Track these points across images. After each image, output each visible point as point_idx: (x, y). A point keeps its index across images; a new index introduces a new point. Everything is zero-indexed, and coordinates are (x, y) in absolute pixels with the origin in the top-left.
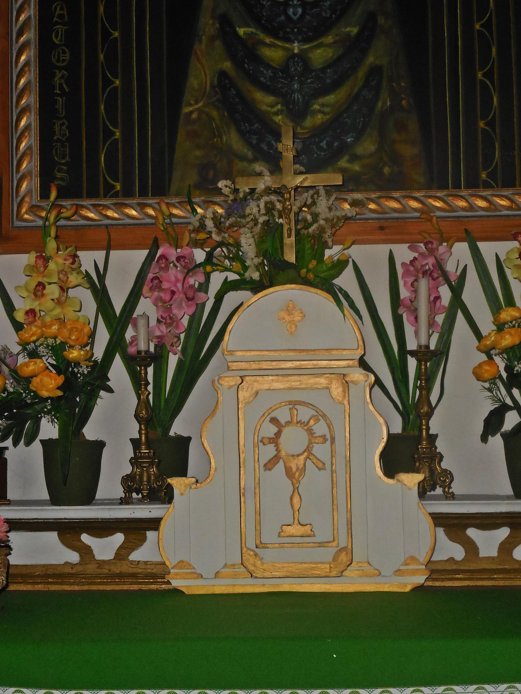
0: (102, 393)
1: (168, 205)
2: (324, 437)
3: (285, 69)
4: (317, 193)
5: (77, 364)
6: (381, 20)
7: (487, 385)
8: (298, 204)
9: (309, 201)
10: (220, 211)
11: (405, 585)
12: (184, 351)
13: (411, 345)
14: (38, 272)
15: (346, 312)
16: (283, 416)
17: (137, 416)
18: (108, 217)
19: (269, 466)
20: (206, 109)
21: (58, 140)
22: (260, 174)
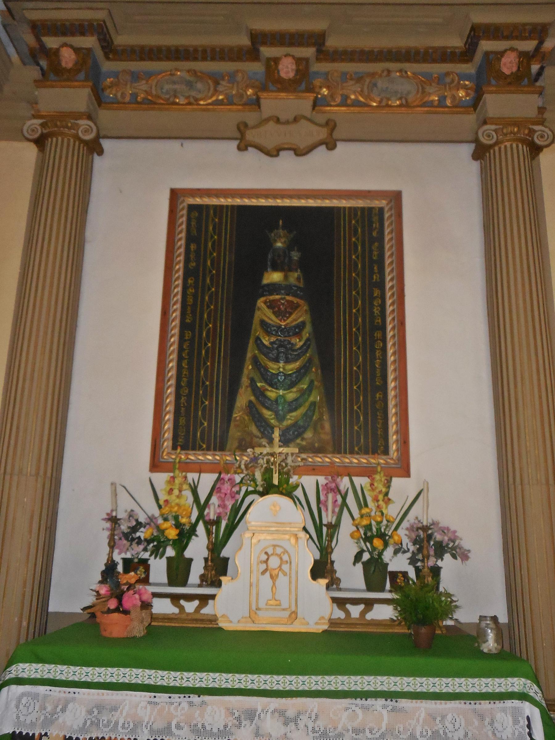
0: (194, 537)
1: (225, 455)
2: (287, 562)
3: (276, 401)
5: (184, 525)
6: (316, 383)
12: (229, 519)
13: (325, 522)
16: (270, 551)
17: (208, 548)
18: (199, 459)
19: (264, 573)
21: (181, 426)
22: (265, 446)
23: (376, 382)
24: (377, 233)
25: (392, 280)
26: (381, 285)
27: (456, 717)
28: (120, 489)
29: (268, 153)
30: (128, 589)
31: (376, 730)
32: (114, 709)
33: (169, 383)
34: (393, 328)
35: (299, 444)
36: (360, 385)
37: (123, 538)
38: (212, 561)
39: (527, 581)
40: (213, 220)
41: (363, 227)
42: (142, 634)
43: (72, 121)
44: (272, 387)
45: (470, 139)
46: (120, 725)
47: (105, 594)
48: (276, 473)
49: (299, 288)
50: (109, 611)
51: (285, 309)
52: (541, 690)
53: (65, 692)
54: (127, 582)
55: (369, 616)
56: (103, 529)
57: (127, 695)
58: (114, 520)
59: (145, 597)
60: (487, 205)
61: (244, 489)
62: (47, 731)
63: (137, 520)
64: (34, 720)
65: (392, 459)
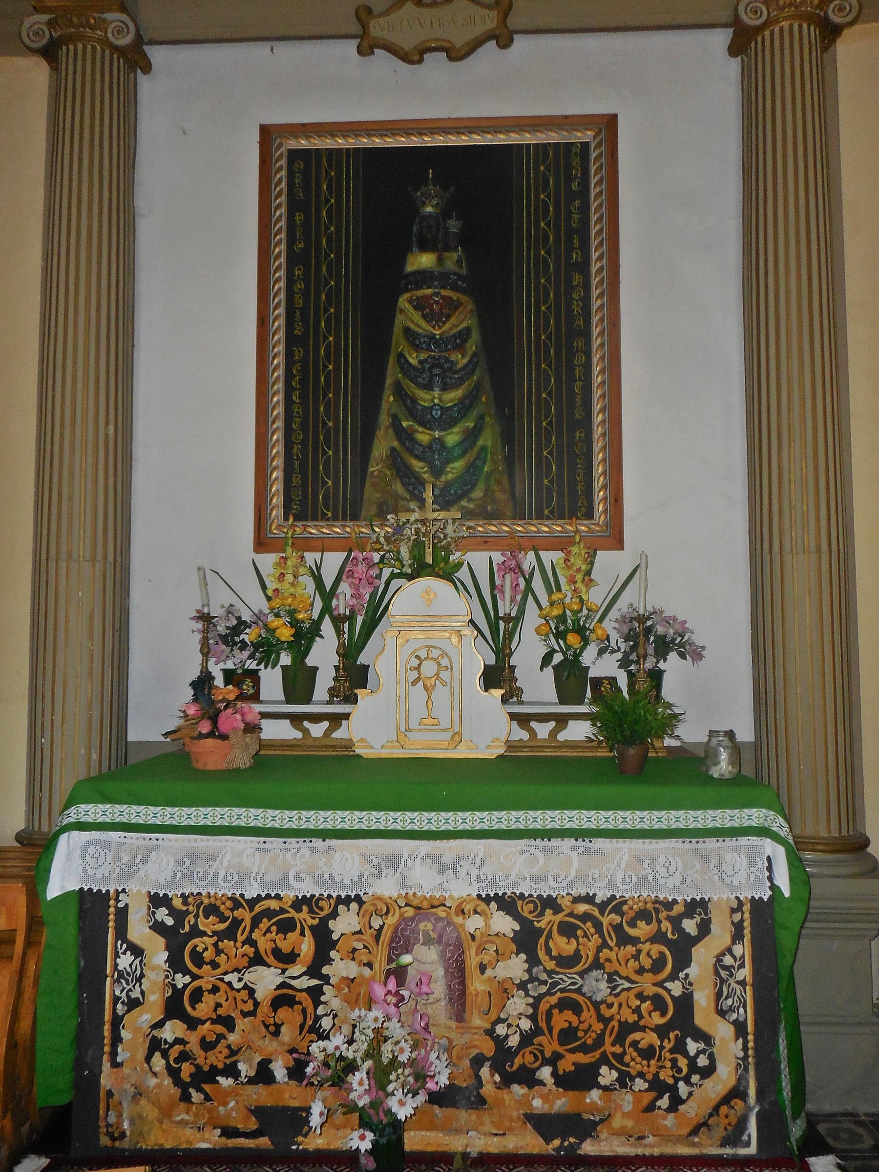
0: (317, 639)
3: (430, 447)
4: (447, 521)
5: (303, 622)
6: (487, 419)
7: (543, 638)
8: (435, 529)
9: (442, 527)
10: (390, 530)
11: (493, 754)
13: (501, 614)
14: (281, 567)
15: (461, 594)
16: (423, 654)
18: (323, 533)
19: (414, 683)
20: (383, 470)
22: (413, 511)
23: (575, 415)
24: (579, 184)
25: (600, 258)
26: (584, 267)
27: (671, 859)
28: (210, 576)
29: (406, 57)
30: (226, 708)
31: (563, 877)
32: (212, 858)
33: (275, 426)
34: (602, 333)
35: (464, 507)
36: (551, 421)
37: (220, 642)
38: (344, 670)
39: (782, 684)
40: (327, 173)
41: (557, 178)
42: (248, 765)
43: (96, 15)
44: (425, 427)
45: (725, 20)
46: (221, 877)
47: (194, 715)
48: (429, 548)
49: (460, 277)
50: (201, 736)
51: (441, 310)
52: (789, 824)
53: (144, 839)
54: (224, 698)
55: (562, 737)
56: (193, 631)
57: (227, 841)
58: (205, 618)
59: (250, 718)
60: (749, 133)
61: (386, 573)
62: (125, 887)
63: (239, 618)
64: (107, 874)
65: (598, 524)
